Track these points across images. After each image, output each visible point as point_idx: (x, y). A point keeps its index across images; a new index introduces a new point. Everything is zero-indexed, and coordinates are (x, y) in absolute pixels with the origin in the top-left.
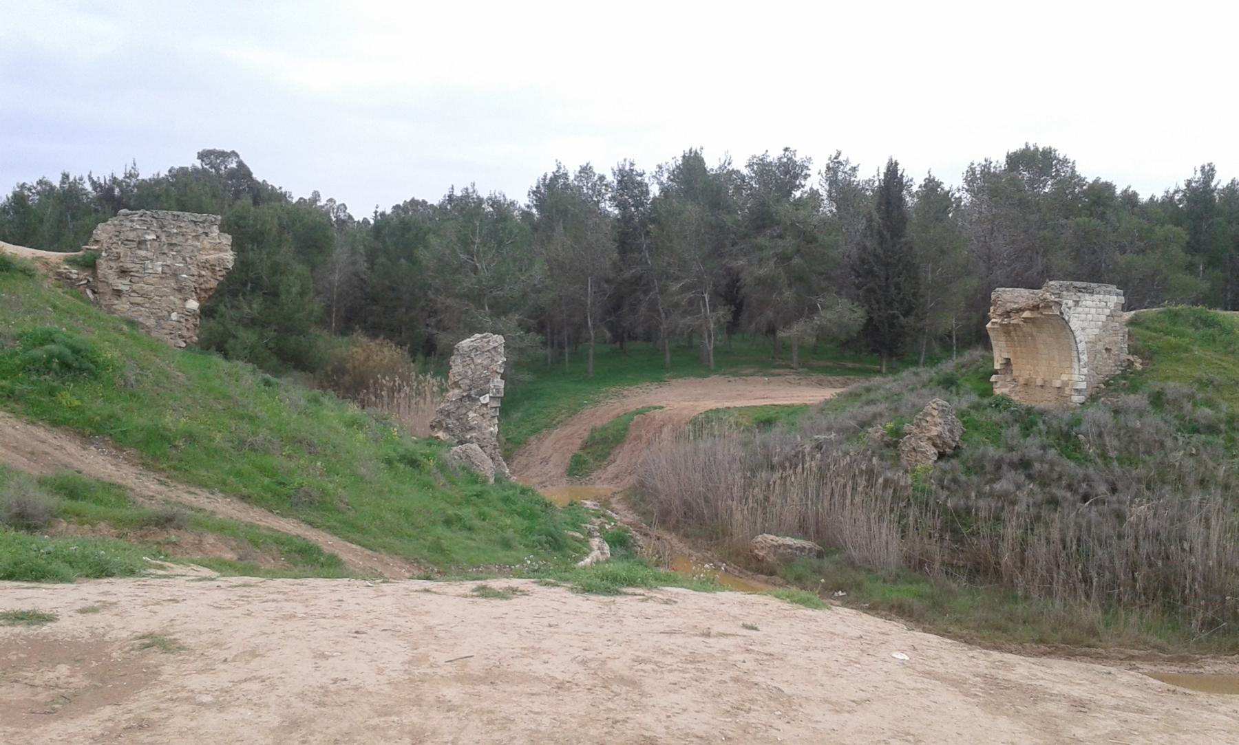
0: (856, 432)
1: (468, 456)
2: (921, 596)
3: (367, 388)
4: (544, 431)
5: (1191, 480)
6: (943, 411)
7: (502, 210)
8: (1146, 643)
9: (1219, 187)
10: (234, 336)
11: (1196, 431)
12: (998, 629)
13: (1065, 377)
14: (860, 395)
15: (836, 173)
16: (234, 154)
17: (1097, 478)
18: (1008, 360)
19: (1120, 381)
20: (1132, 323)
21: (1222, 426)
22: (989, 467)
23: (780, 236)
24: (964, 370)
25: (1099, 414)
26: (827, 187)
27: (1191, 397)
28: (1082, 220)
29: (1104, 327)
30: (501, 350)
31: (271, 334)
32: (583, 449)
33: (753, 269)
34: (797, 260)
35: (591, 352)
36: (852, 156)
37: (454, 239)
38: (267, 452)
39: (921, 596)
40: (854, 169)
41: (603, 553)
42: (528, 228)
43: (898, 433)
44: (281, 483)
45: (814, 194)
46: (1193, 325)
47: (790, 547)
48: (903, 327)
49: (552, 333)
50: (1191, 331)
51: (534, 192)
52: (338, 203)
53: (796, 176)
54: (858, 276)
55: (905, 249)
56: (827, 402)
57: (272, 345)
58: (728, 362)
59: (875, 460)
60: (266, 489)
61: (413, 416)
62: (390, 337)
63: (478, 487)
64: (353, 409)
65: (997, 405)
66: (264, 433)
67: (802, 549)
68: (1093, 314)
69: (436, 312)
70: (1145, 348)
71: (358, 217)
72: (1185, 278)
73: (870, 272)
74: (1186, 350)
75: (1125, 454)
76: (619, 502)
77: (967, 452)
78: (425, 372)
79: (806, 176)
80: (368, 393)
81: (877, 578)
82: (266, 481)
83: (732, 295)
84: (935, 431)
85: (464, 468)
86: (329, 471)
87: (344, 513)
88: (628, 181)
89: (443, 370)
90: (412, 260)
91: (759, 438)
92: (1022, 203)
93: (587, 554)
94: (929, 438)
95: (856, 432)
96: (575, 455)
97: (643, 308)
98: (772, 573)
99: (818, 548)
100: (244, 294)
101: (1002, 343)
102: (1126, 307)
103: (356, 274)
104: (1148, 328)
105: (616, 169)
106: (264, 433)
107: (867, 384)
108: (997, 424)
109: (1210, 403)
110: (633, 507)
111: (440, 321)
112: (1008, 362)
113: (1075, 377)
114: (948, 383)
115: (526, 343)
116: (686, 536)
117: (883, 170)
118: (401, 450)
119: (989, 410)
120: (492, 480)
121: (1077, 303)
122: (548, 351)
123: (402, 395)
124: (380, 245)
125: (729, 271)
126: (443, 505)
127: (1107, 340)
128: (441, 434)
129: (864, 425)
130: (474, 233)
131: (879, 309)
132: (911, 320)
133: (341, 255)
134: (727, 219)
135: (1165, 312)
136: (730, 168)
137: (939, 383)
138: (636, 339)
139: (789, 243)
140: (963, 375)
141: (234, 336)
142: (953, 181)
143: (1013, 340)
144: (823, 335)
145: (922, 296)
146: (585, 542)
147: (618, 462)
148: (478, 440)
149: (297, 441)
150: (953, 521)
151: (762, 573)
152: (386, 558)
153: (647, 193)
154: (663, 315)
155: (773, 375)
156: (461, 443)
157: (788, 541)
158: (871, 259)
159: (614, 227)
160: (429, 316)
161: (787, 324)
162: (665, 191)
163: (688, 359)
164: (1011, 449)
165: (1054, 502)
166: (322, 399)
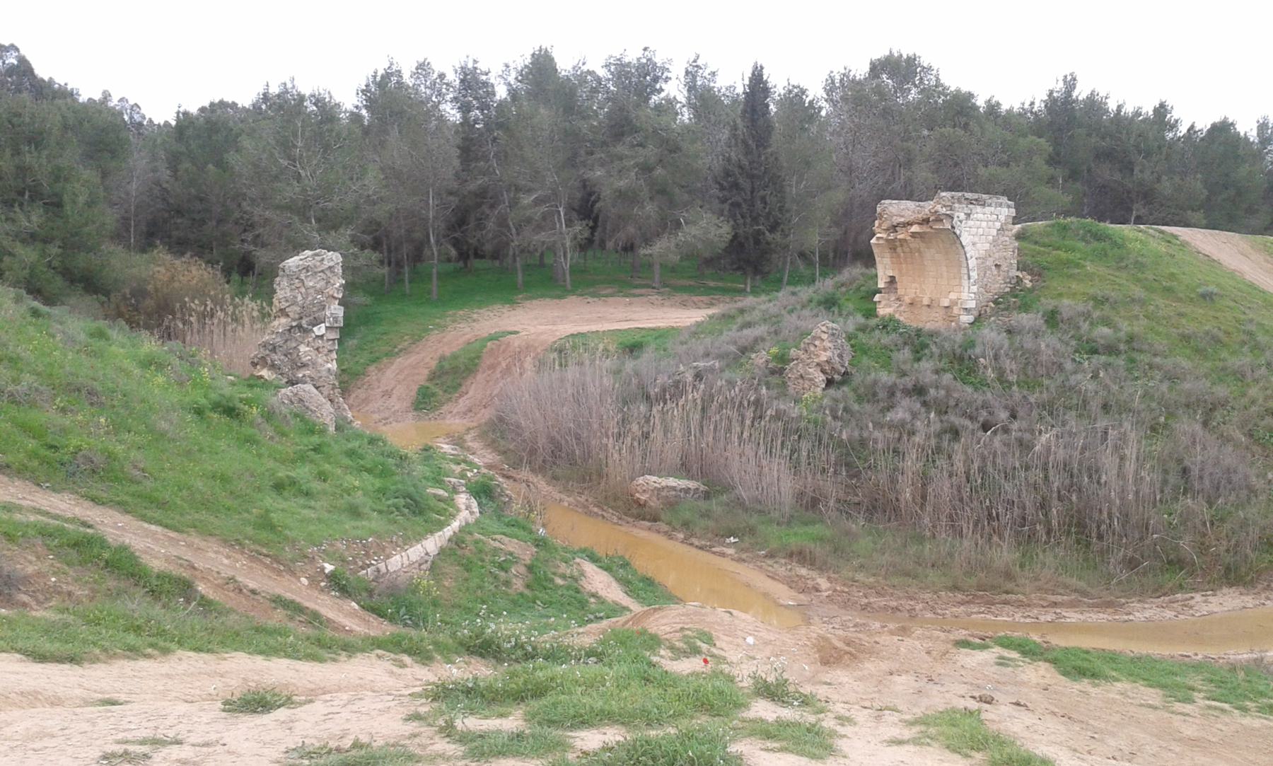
0: (736, 358)
1: (301, 400)
2: (821, 539)
3: (173, 313)
4: (385, 360)
5: (1095, 405)
6: (833, 335)
7: (327, 111)
8: (1066, 587)
9: (1080, 98)
10: (10, 254)
11: (1094, 351)
12: (907, 574)
13: (953, 296)
14: (733, 317)
15: (694, 77)
16: (13, 47)
17: (997, 404)
18: (893, 278)
19: (1009, 300)
20: (1019, 237)
21: (1122, 347)
22: (882, 395)
23: (641, 145)
24: (844, 289)
25: (990, 335)
26: (686, 93)
27: (1087, 316)
28: (948, 130)
29: (995, 243)
30: (339, 270)
31: (54, 250)
32: (430, 379)
33: (610, 180)
34: (659, 171)
35: (434, 271)
36: (710, 62)
37: (273, 142)
38: (33, 405)
39: (821, 539)
40: (713, 74)
41: (472, 513)
42: (358, 131)
43: (783, 359)
44: (52, 447)
45: (671, 102)
46: (1083, 239)
47: (674, 488)
48: (768, 243)
49: (389, 251)
50: (1081, 245)
51: (363, 91)
52: (131, 102)
53: (656, 79)
54: (722, 188)
55: (771, 159)
56: (698, 324)
57: (56, 263)
58: (585, 282)
59: (764, 391)
60: (33, 455)
61: (231, 345)
62: (200, 255)
63: (315, 439)
64: (149, 344)
65: (885, 327)
66: (28, 379)
67: (687, 490)
68: (984, 227)
69: (252, 226)
70: (1036, 263)
71: (159, 119)
72: (1047, 191)
73: (736, 186)
74: (1078, 266)
75: (1022, 377)
76: (474, 439)
77: (857, 379)
78: (242, 294)
79: (667, 80)
80: (174, 318)
81: (771, 521)
82: (32, 444)
83: (586, 207)
84: (824, 357)
85: (296, 415)
86: (117, 428)
87: (139, 483)
88: (472, 83)
89: (266, 293)
90: (221, 164)
91: (630, 365)
92: (886, 113)
93: (453, 516)
94: (818, 364)
95: (736, 358)
96: (422, 387)
97: (491, 225)
98: (655, 519)
99: (702, 488)
100: (21, 205)
101: (887, 260)
102: (1016, 220)
103: (158, 183)
104: (1036, 243)
105: (458, 66)
106: (28, 379)
107: (740, 305)
108: (885, 347)
109: (1106, 322)
110: (492, 445)
111: (258, 236)
112: (892, 280)
113: (965, 296)
114: (829, 303)
115: (362, 261)
116: (555, 478)
117: (748, 74)
118: (214, 396)
119: (877, 332)
120: (332, 429)
121: (968, 215)
122: (385, 270)
123: (216, 321)
124: (183, 149)
125: (584, 184)
126: (271, 464)
127: (997, 255)
128: (265, 373)
129: (744, 350)
130: (295, 135)
131: (745, 224)
132: (778, 236)
133: (139, 161)
134: (584, 126)
135: (1053, 226)
136: (585, 68)
137: (820, 303)
138: (482, 257)
139: (650, 152)
140: (844, 294)
141: (10, 254)
142: (815, 91)
143: (899, 256)
144: (689, 255)
145: (788, 211)
146: (450, 501)
147: (471, 393)
148: (312, 379)
149: (74, 389)
150: (848, 454)
151: (644, 519)
152: (197, 541)
153: (494, 95)
154: (514, 231)
155: (635, 296)
156: (292, 383)
157: (672, 482)
158: (737, 171)
159: (457, 132)
160: (245, 231)
161: (648, 241)
162: (513, 93)
163: (540, 278)
164: (903, 374)
165: (955, 433)
166: (109, 332)
